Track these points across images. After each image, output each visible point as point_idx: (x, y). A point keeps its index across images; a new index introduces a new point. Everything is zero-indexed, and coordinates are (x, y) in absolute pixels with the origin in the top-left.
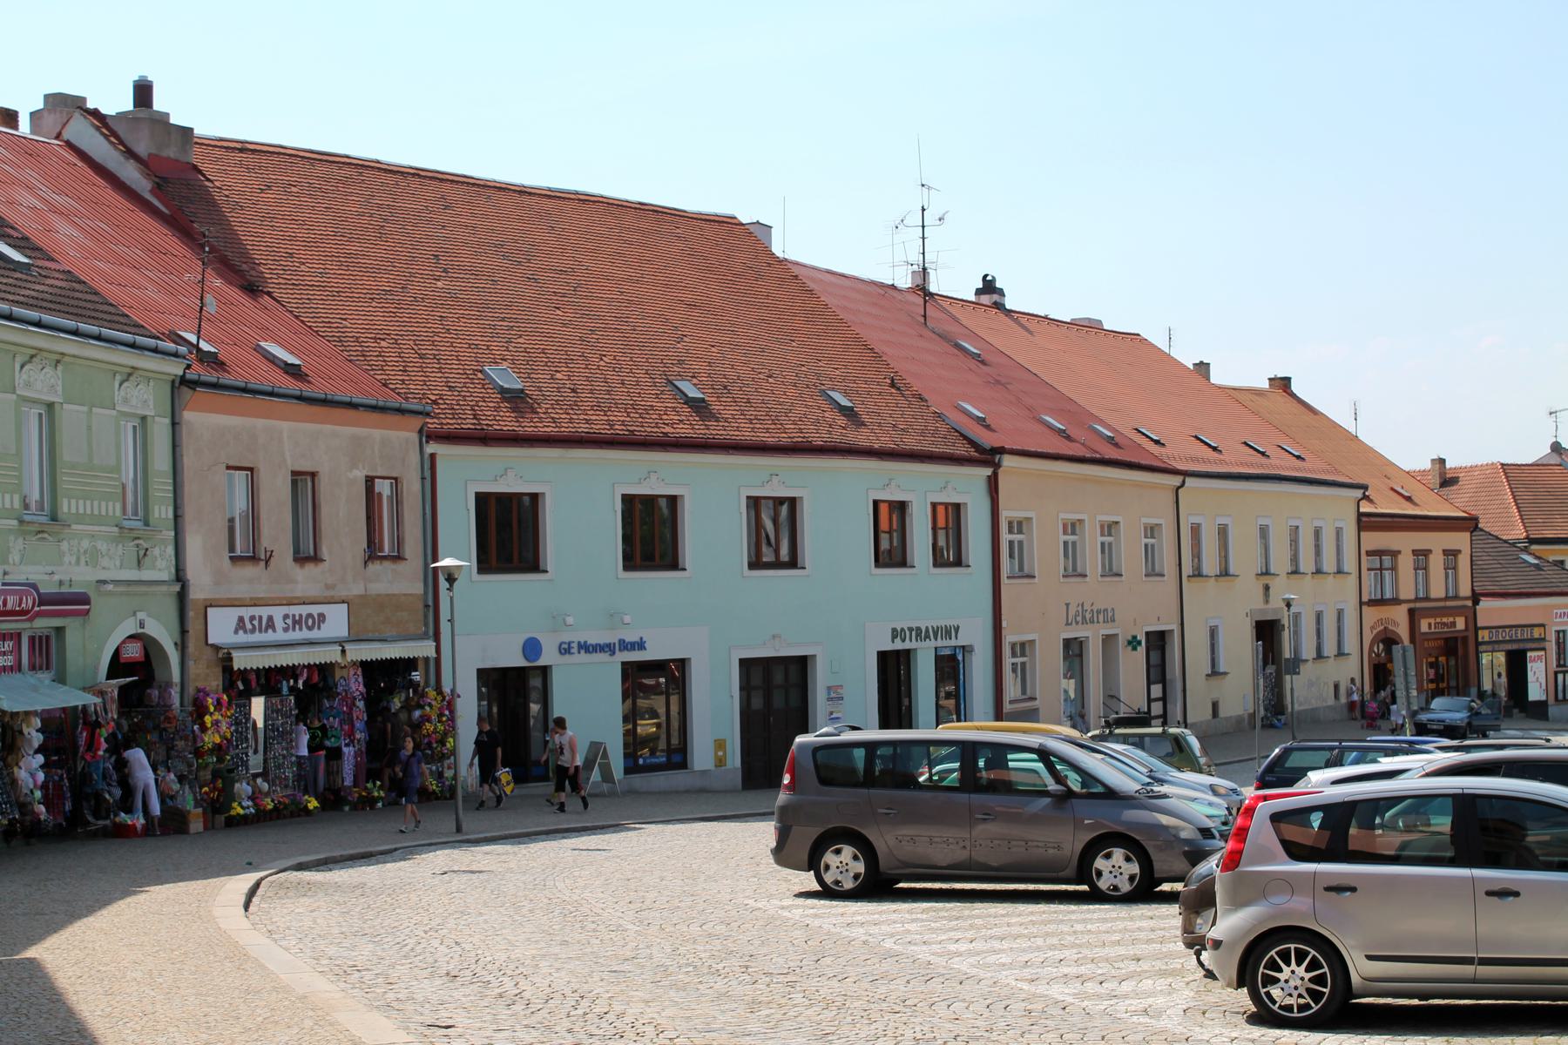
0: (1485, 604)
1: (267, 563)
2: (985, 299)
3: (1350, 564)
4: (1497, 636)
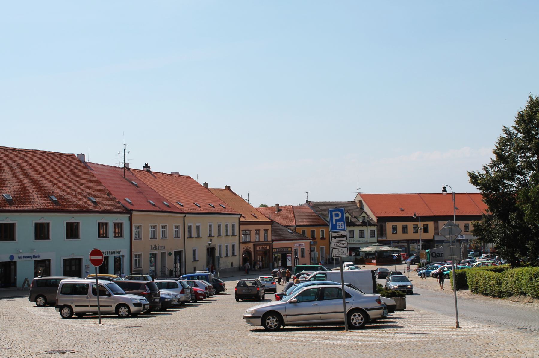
0: (275, 242)
2: (145, 169)
3: (236, 233)
4: (278, 250)
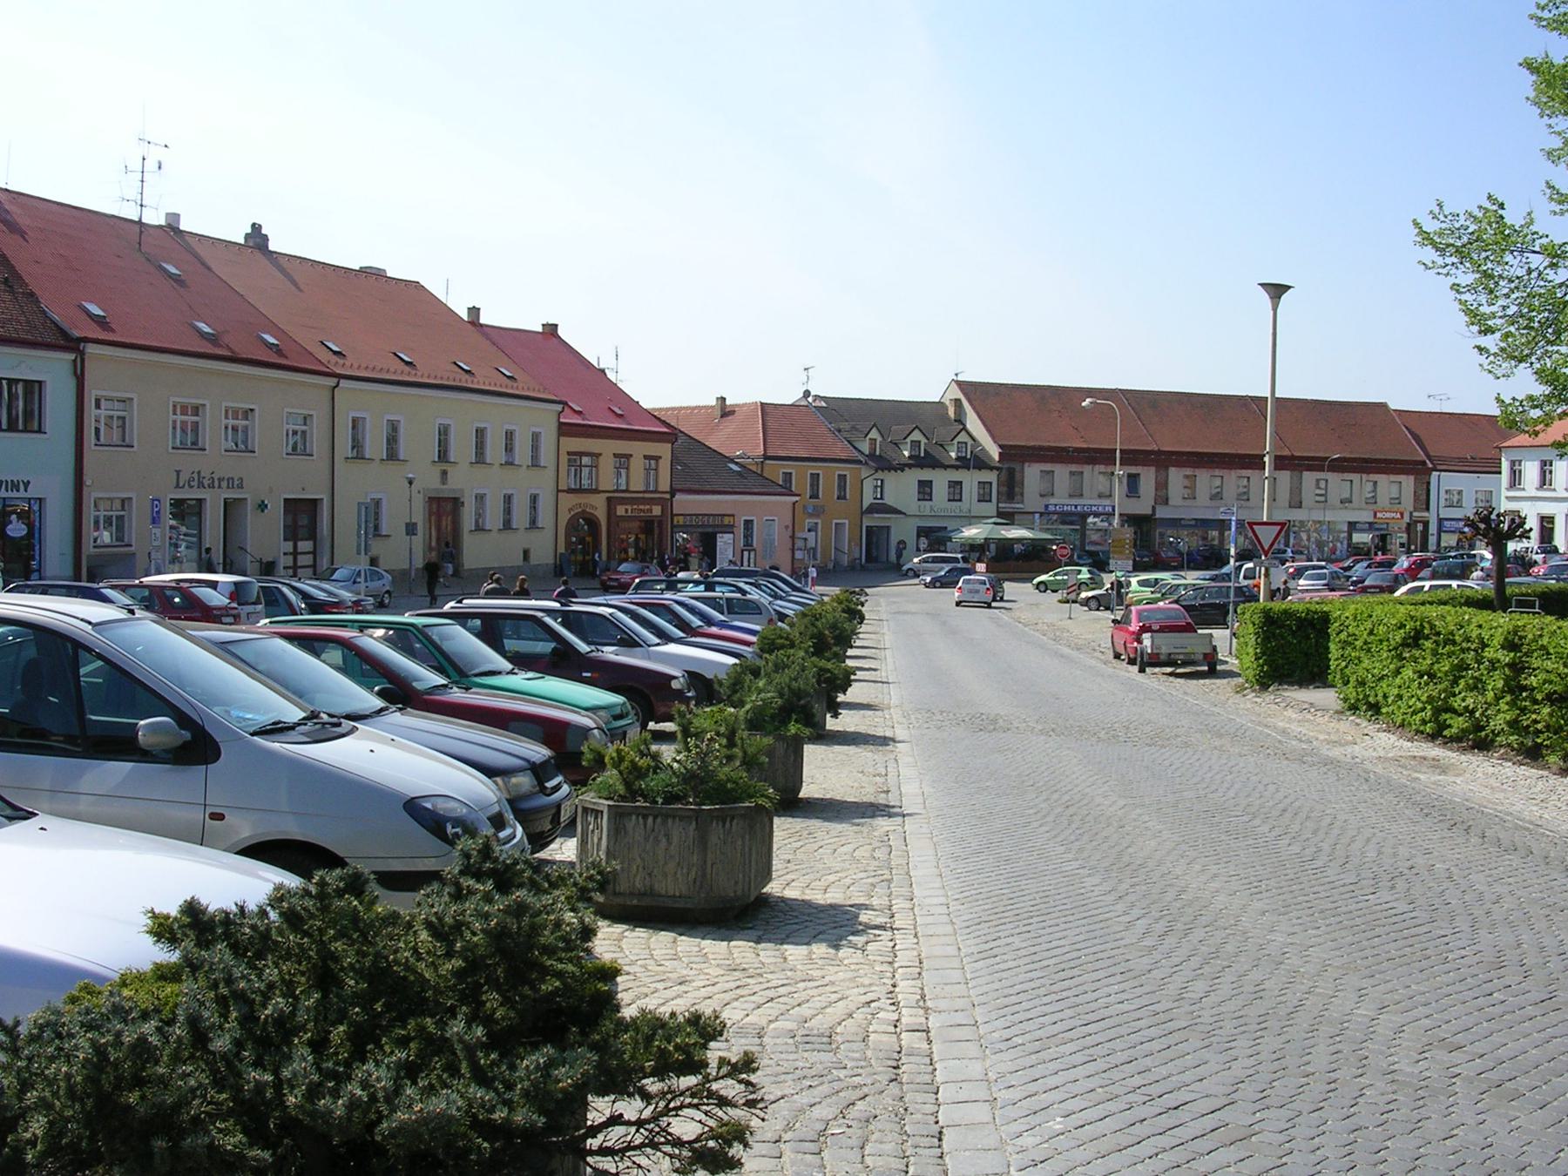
0: (678, 497)
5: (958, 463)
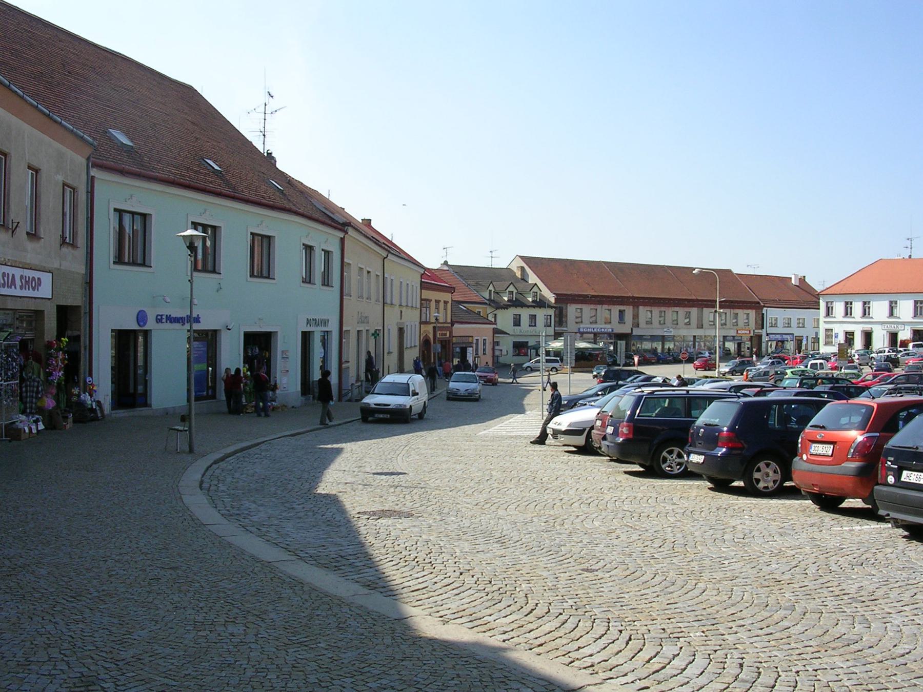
1: (13, 232)
5: (534, 304)
